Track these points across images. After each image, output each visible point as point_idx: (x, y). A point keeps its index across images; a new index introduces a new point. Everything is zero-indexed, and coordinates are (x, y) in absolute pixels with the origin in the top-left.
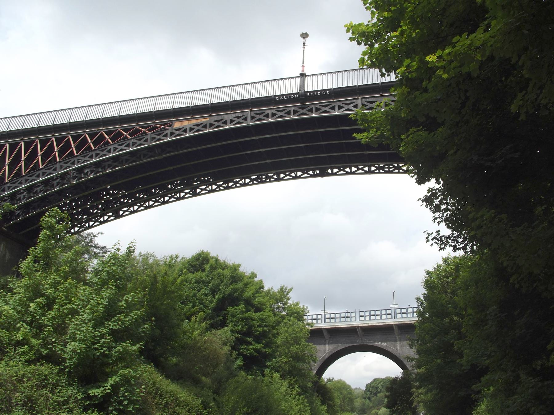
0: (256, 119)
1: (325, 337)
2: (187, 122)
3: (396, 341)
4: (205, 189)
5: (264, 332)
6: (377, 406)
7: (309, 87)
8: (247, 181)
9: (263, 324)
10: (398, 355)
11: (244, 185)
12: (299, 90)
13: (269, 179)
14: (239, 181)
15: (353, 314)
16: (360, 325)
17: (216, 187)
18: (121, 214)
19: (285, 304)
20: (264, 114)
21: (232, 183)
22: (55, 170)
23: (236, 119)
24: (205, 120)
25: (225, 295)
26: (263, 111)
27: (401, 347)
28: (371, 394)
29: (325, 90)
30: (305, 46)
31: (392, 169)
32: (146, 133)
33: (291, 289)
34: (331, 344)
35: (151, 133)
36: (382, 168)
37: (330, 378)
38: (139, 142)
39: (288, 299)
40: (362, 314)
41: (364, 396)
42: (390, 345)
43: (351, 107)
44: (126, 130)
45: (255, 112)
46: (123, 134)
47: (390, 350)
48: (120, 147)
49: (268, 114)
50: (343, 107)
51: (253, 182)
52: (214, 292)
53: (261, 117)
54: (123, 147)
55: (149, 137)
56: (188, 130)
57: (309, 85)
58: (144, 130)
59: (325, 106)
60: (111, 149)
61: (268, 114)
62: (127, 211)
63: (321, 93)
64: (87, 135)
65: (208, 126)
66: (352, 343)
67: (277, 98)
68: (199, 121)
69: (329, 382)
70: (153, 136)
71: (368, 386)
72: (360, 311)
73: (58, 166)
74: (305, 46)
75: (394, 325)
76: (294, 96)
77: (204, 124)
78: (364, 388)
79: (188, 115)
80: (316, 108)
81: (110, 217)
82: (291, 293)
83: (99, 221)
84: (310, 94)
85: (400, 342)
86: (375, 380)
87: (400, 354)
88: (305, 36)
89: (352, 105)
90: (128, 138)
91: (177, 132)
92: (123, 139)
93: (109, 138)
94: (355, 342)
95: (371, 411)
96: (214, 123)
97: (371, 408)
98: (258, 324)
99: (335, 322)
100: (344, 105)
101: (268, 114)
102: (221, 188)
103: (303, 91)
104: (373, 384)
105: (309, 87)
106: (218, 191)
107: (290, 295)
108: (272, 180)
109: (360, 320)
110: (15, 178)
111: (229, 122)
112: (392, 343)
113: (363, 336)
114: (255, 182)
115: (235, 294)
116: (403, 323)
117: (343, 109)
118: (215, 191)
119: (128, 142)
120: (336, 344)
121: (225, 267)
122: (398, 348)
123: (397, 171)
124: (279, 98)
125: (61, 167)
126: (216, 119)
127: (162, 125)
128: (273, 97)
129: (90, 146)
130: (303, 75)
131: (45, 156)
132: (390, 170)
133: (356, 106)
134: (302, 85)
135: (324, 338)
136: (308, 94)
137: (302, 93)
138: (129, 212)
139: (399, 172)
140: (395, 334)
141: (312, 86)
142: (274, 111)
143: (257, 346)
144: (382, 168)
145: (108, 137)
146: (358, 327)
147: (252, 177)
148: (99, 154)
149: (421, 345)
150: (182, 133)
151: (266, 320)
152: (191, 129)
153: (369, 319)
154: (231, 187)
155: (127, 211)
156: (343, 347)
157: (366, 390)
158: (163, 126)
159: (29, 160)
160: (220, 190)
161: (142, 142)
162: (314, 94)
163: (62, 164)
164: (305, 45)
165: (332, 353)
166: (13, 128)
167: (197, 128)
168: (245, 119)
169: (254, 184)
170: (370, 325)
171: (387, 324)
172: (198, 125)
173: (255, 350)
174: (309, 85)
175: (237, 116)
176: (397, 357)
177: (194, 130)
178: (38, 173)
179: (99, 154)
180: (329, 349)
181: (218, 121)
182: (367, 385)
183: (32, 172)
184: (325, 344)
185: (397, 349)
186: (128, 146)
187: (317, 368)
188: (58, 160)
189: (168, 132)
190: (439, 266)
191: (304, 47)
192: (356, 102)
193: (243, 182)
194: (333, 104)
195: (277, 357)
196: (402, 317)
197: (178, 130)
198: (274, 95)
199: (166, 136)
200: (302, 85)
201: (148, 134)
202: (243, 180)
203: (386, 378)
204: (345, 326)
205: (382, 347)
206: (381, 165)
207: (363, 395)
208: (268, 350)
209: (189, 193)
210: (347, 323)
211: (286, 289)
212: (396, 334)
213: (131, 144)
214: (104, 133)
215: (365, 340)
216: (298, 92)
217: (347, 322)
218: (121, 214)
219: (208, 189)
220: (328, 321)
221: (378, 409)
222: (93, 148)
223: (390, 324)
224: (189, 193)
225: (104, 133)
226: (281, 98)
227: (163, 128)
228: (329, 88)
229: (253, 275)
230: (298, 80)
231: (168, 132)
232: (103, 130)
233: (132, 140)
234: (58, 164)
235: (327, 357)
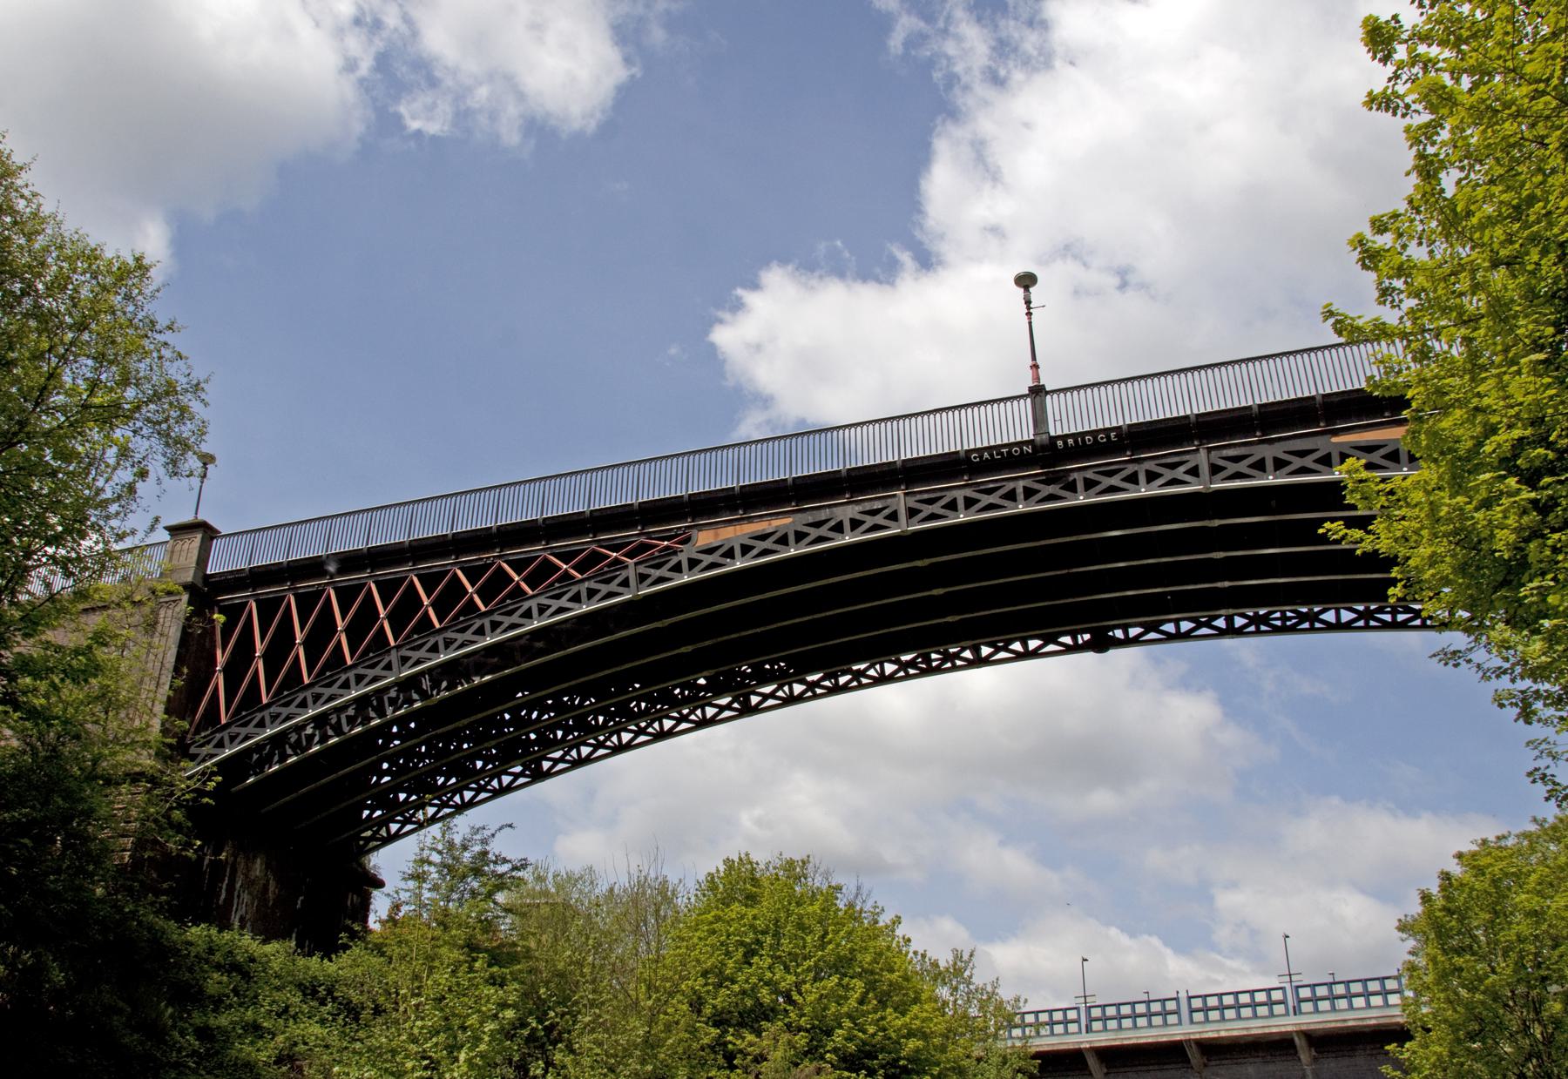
4: (772, 695)
7: (1058, 423)
8: (889, 668)
11: (883, 679)
12: (1032, 432)
13: (950, 663)
14: (867, 669)
16: (1192, 1037)
18: (545, 768)
21: (848, 677)
22: (388, 667)
23: (867, 518)
29: (1106, 431)
31: (1294, 621)
32: (623, 562)
35: (636, 564)
36: (1265, 620)
38: (605, 589)
40: (1197, 1003)
43: (1180, 473)
44: (566, 557)
45: (919, 497)
46: (559, 568)
48: (555, 604)
49: (1013, 491)
50: (1159, 475)
51: (907, 673)
54: (563, 602)
55: (631, 573)
56: (738, 551)
57: (1058, 418)
58: (615, 554)
59: (1110, 474)
60: (530, 609)
61: (955, 499)
62: (562, 759)
64: (459, 573)
65: (792, 538)
67: (975, 458)
70: (642, 569)
73: (394, 657)
75: (1294, 1034)
76: (1022, 450)
79: (734, 510)
80: (965, 498)
81: (517, 776)
83: (489, 787)
89: (1182, 469)
90: (573, 577)
91: (708, 559)
92: (559, 580)
93: (525, 580)
96: (806, 530)
101: (955, 499)
102: (819, 691)
103: (1044, 436)
105: (1058, 423)
106: (809, 699)
108: (959, 663)
109: (1192, 1022)
110: (286, 693)
111: (847, 525)
114: (912, 671)
118: (800, 699)
119: (575, 589)
123: (1306, 625)
124: (981, 457)
125: (404, 660)
126: (811, 520)
127: (663, 539)
128: (962, 454)
129: (471, 600)
130: (1037, 391)
131: (355, 633)
132: (1288, 623)
133: (1194, 472)
134: (1039, 418)
136: (1060, 443)
137: (1042, 440)
138: (568, 762)
139: (1312, 629)
141: (1065, 420)
142: (969, 492)
144: (1265, 620)
145: (519, 575)
148: (501, 623)
150: (721, 560)
152: (746, 549)
153: (1137, 1006)
154: (845, 688)
155: (562, 759)
158: (666, 543)
159: (314, 645)
160: (816, 696)
161: (613, 587)
163: (404, 652)
166: (263, 559)
168: (894, 516)
169: (908, 677)
170: (1223, 1034)
172: (763, 537)
174: (1058, 418)
175: (868, 509)
177: (755, 552)
178: (344, 677)
179: (501, 623)
181: (818, 525)
183: (328, 674)
186: (576, 599)
188: (392, 643)
191: (1029, 314)
192: (1192, 461)
196: (1317, 1011)
197: (710, 551)
198: (966, 448)
199: (677, 568)
200: (1039, 418)
201: (627, 567)
204: (1150, 1040)
206: (1262, 612)
209: (728, 707)
210: (1154, 1032)
213: (584, 595)
214: (505, 566)
216: (1032, 437)
217: (1152, 1030)
218: (545, 768)
219: (780, 693)
220: (1097, 1025)
222: (483, 609)
224: (728, 707)
225: (505, 566)
226: (986, 455)
227: (667, 548)
231: (683, 558)
232: (499, 559)
233: (586, 584)
234: (394, 652)
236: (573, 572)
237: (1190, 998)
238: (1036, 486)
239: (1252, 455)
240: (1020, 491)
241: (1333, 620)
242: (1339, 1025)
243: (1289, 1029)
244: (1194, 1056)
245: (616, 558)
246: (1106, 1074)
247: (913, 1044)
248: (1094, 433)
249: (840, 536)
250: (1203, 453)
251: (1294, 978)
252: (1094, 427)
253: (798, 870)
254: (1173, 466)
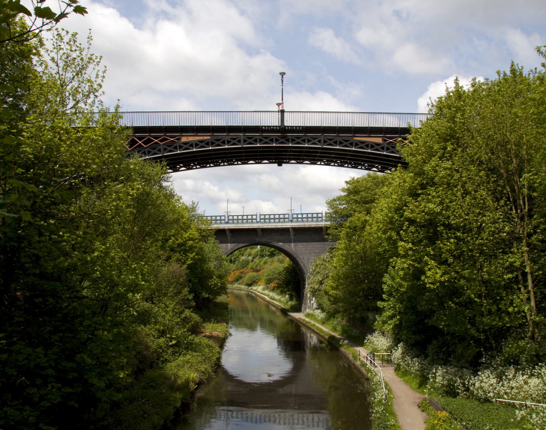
10: (291, 253)
15: (254, 217)
24: (206, 137)
27: (295, 246)
29: (299, 127)
32: (159, 143)
34: (233, 242)
40: (262, 217)
45: (247, 137)
47: (286, 249)
65: (210, 143)
89: (317, 140)
90: (143, 146)
91: (185, 146)
96: (215, 141)
117: (311, 143)
126: (216, 139)
133: (319, 141)
136: (287, 128)
141: (290, 121)
150: (189, 147)
168: (239, 141)
170: (269, 227)
171: (285, 227)
172: (202, 141)
176: (291, 254)
185: (291, 248)
197: (186, 143)
226: (290, 128)
227: (172, 141)
228: (302, 125)
233: (147, 149)
236: (142, 144)
237: (260, 215)
238: (279, 139)
239: (221, 139)
240: (274, 139)
242: (303, 226)
243: (289, 227)
244: (260, 233)
245: (156, 142)
247: (191, 242)
248: (296, 127)
250: (322, 137)
251: (292, 211)
252: (296, 125)
254: (314, 139)
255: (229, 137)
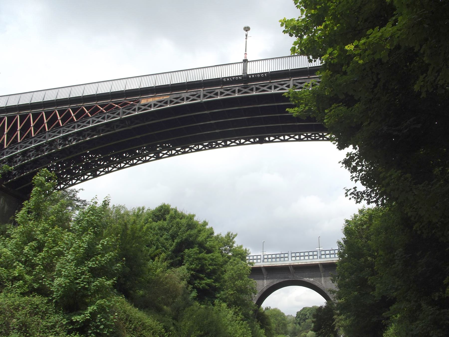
0: (207, 97)
1: (264, 273)
2: (152, 99)
3: (321, 277)
4: (166, 154)
5: (214, 269)
6: (305, 329)
7: (250, 71)
8: (201, 147)
9: (213, 263)
10: (322, 289)
11: (198, 150)
12: (242, 73)
13: (218, 146)
14: (194, 147)
15: (286, 255)
16: (291, 264)
17: (175, 152)
18: (98, 174)
19: (231, 247)
20: (214, 93)
21: (188, 149)
22: (45, 138)
23: (191, 97)
24: (166, 97)
25: (183, 239)
26: (213, 90)
27: (325, 282)
28: (301, 320)
29: (264, 73)
30: (247, 38)
31: (318, 137)
32: (119, 108)
33: (236, 235)
34: (269, 279)
35: (123, 108)
36: (310, 137)
37: (267, 307)
38: (112, 116)
39: (233, 243)
40: (293, 255)
41: (295, 321)
42: (316, 281)
43: (284, 87)
44: (102, 106)
45: (207, 91)
46: (100, 109)
47: (316, 284)
48: (97, 120)
49: (217, 93)
50: (278, 87)
51: (205, 148)
52: (173, 237)
53: (212, 95)
54: (100, 119)
55: (121, 111)
56: (153, 105)
57: (250, 69)
58: (117, 105)
59: (264, 86)
60: (90, 121)
61: (217, 92)
62: (103, 171)
63: (260, 76)
64: (70, 110)
65: (169, 102)
66: (285, 278)
67: (225, 80)
68: (161, 98)
69: (267, 310)
70: (124, 110)
71: (298, 314)
72: (292, 252)
73: (47, 135)
74: (247, 38)
75: (319, 264)
76: (239, 78)
77: (165, 101)
78: (295, 315)
79: (152, 93)
80: (256, 87)
81: (89, 176)
82: (236, 238)
83: (80, 179)
84: (252, 77)
85: (324, 278)
86: (304, 308)
87: (324, 287)
88: (247, 29)
89: (285, 85)
90: (104, 112)
91: (143, 108)
92: (100, 113)
93: (88, 112)
94: (288, 278)
95: (301, 334)
96: (173, 100)
97: (301, 331)
98: (209, 263)
99: (272, 261)
100: (279, 86)
101: (217, 92)
102: (179, 153)
103: (245, 74)
104: (303, 312)
105: (250, 71)
106: (177, 155)
107: (235, 240)
108: (220, 146)
109: (292, 260)
110: (12, 145)
111: (185, 99)
112: (318, 278)
113: (295, 273)
114: (207, 148)
115: (191, 239)
116: (326, 262)
117: (278, 89)
118: (174, 155)
119: (103, 116)
120: (272, 279)
121: (182, 216)
122: (323, 282)
123: (322, 139)
124: (226, 80)
125: (50, 135)
126: (175, 97)
127: (131, 101)
128: (221, 79)
129: (73, 118)
130: (245, 61)
131: (36, 127)
132: (316, 138)
133: (288, 86)
134: (245, 69)
135: (263, 274)
136: (250, 76)
137: (244, 75)
138: (104, 172)
139: (323, 140)
140: (320, 271)
141: (253, 69)
143: (209, 281)
144: (310, 137)
145: (88, 111)
146: (290, 265)
147: (204, 144)
148: (80, 125)
149: (341, 280)
150: (147, 108)
151: (216, 259)
152: (155, 105)
154: (187, 152)
155: (103, 171)
156: (278, 282)
157: (297, 316)
158: (132, 102)
159: (23, 130)
160: (178, 154)
161: (115, 115)
162: (255, 76)
163: (50, 133)
164: (247, 36)
165: (269, 287)
166: (10, 104)
167: (159, 104)
168: (199, 97)
169: (205, 149)
170: (300, 264)
171: (314, 263)
172: (160, 102)
173: (206, 284)
174: (250, 69)
175: (192, 94)
176: (322, 290)
177: (157, 106)
179: (80, 125)
180: (267, 283)
181: (177, 98)
182: (297, 313)
183: (26, 139)
184: (263, 279)
185: (321, 283)
186: (104, 118)
187: (257, 299)
188: (47, 130)
189: (136, 107)
190: (356, 216)
191: (246, 38)
192: (288, 83)
193: (197, 148)
194: (270, 85)
195: (225, 290)
196: (326, 258)
197: (144, 105)
198: (222, 77)
199: (134, 110)
200: (245, 69)
201: (120, 109)
202: (197, 146)
203: (313, 307)
204: (280, 265)
205: (310, 282)
206: (309, 134)
207: (294, 321)
208: (217, 285)
209: (153, 157)
210: (281, 263)
211: (232, 234)
212: (321, 272)
213: (106, 117)
214: (84, 108)
215: (296, 276)
216: (242, 74)
217: (281, 262)
218: (98, 174)
219: (168, 153)
220: (266, 260)
221: (306, 332)
222: (76, 120)
223: (316, 263)
224: (153, 157)
225: (84, 108)
226: (228, 79)
227: (132, 104)
228: (267, 71)
229: (205, 224)
230: (241, 65)
231: (136, 107)
232: (83, 106)
233: (107, 114)
234: (47, 133)
235: (265, 290)
241: (283, 139)
246: (267, 274)
249: (234, 94)
253: (415, 293)
255: (189, 94)
